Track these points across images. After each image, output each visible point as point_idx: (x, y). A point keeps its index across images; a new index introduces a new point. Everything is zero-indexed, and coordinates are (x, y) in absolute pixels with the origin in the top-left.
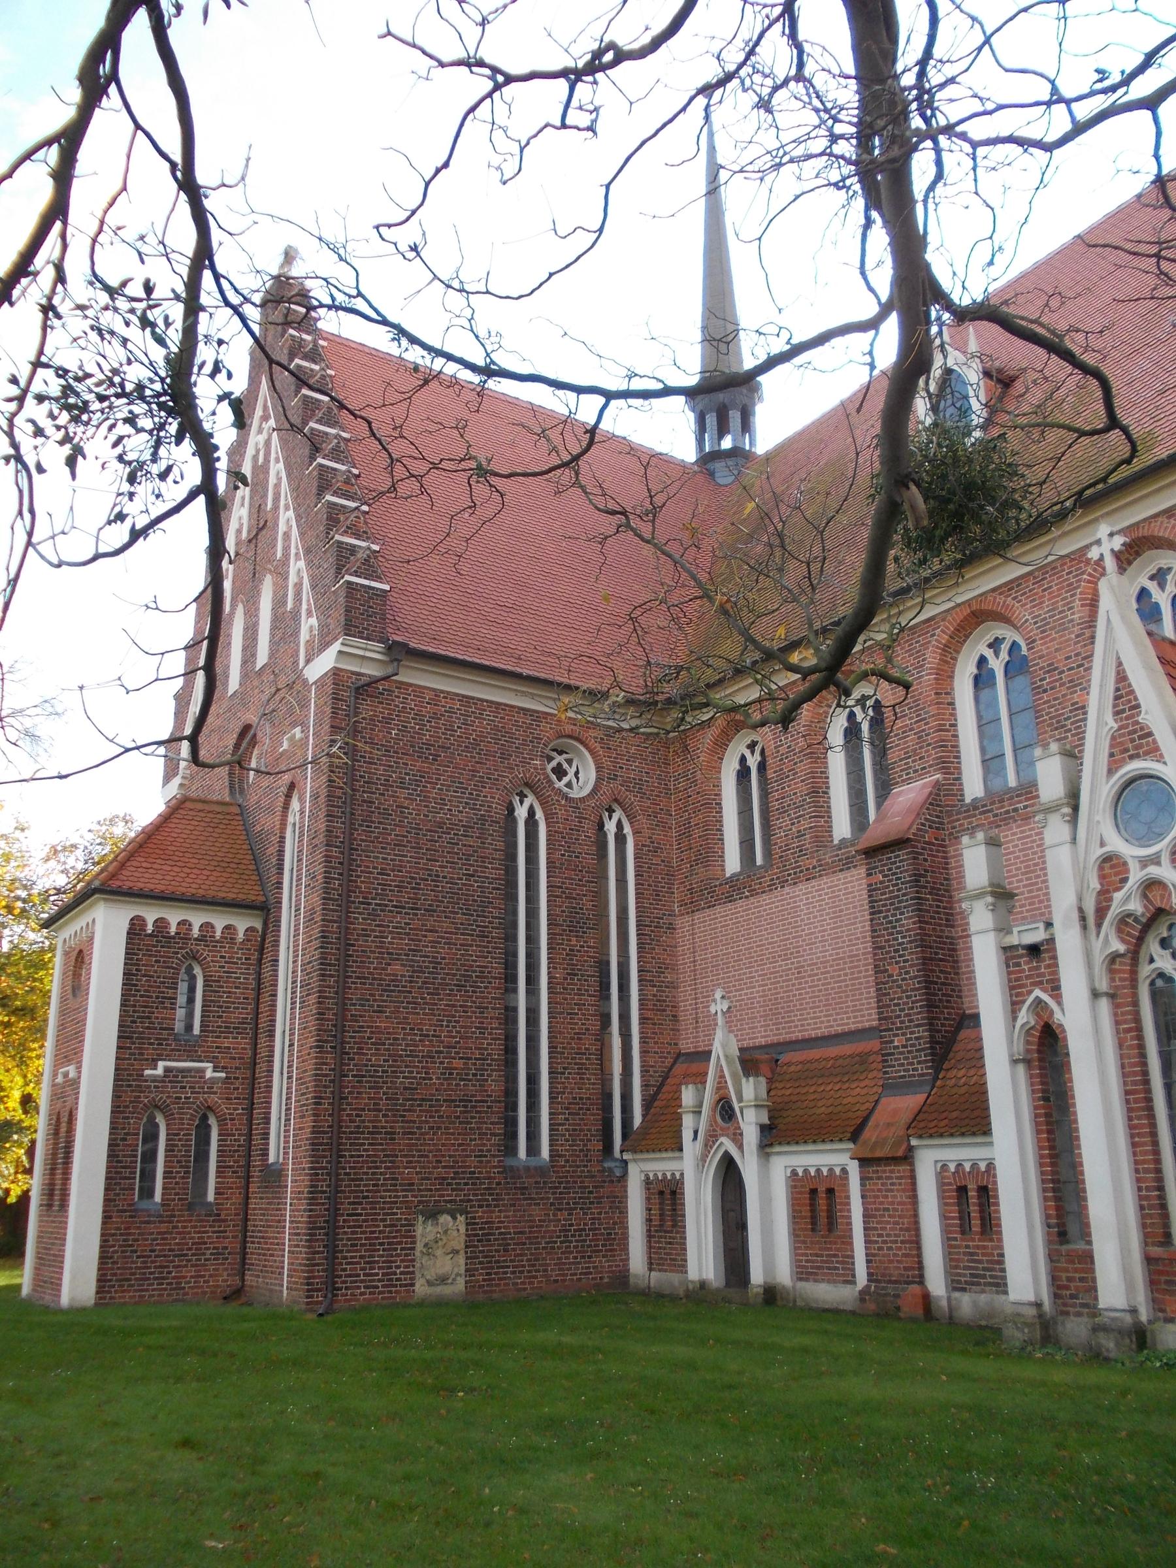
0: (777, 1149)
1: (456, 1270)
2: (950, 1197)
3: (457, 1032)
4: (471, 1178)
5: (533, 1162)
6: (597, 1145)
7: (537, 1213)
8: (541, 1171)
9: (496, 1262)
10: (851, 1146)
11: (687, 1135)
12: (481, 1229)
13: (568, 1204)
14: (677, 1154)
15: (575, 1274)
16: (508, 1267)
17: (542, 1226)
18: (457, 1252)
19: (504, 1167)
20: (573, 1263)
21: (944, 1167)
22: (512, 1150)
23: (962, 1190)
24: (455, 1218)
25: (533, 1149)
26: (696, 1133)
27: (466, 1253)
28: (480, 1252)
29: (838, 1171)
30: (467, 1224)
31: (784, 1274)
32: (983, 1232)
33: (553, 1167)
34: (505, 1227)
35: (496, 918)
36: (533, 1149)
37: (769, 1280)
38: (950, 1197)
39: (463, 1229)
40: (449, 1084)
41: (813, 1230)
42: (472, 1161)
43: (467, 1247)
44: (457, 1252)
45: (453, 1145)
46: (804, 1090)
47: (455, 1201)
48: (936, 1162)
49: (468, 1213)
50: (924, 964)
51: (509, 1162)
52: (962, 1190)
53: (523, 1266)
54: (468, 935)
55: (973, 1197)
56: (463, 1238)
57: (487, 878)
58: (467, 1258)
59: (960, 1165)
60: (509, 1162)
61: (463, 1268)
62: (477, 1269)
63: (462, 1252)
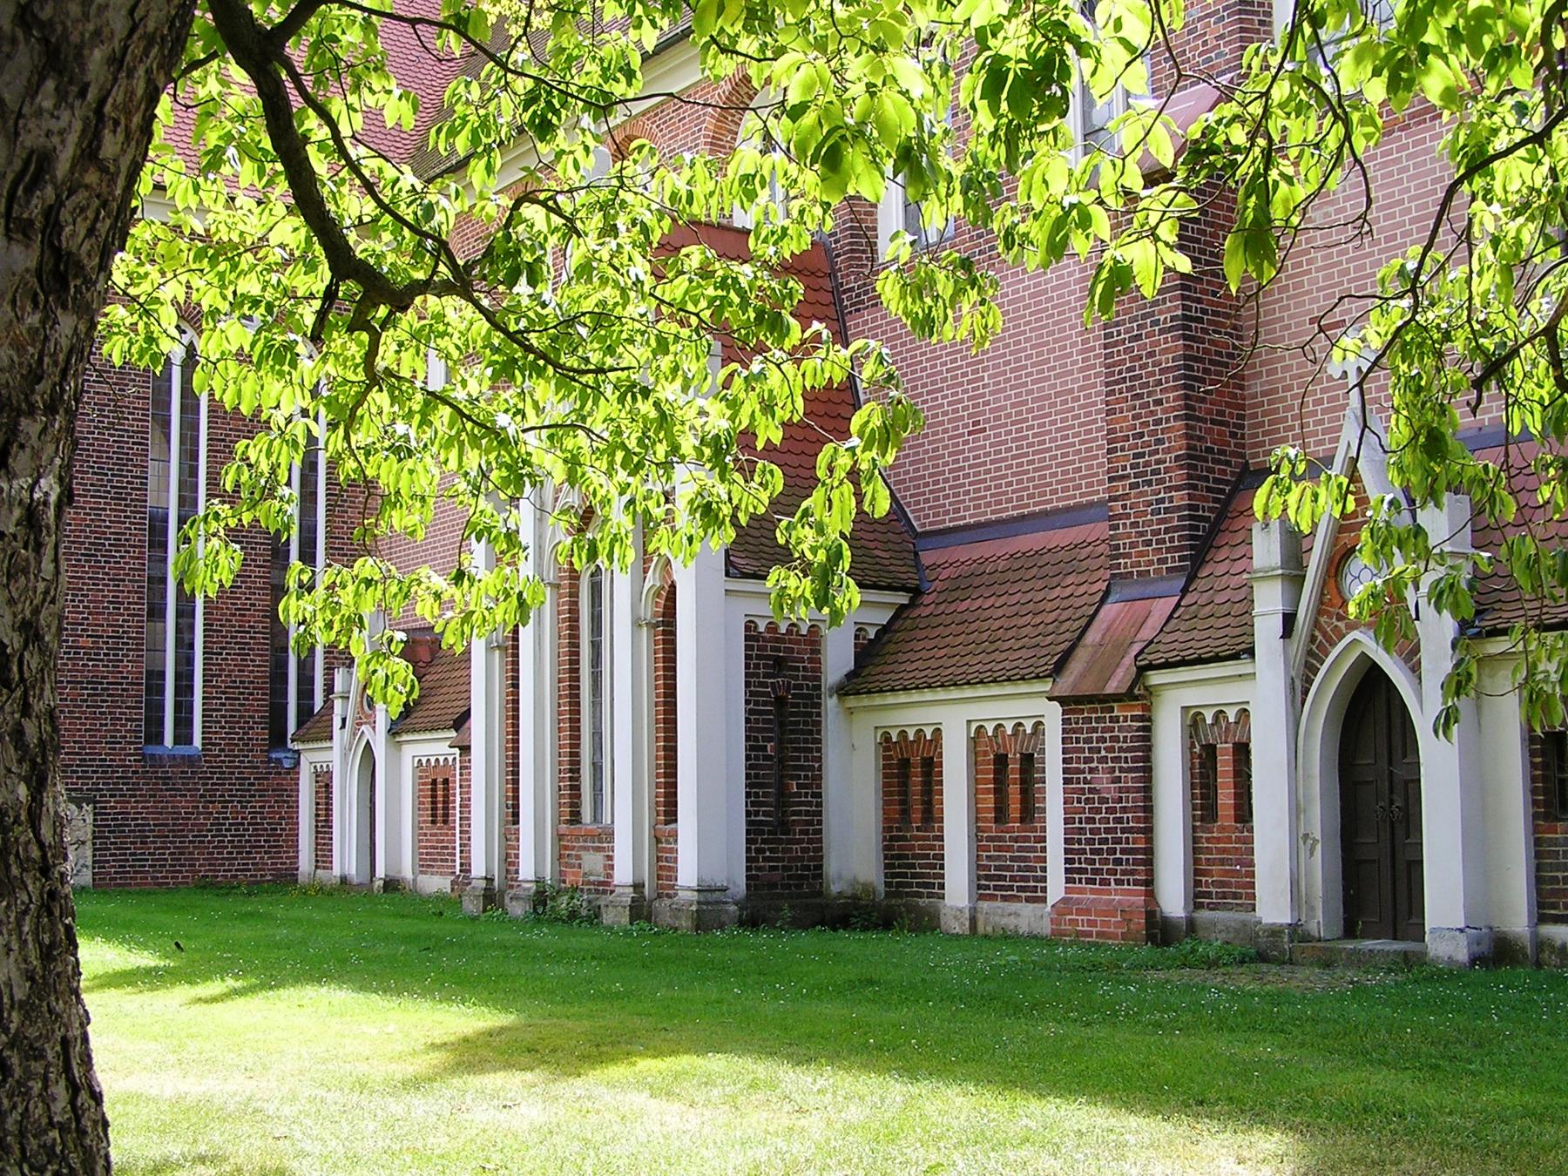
0: (405, 737)
1: (81, 862)
2: (424, 797)
3: (84, 607)
4: (101, 766)
5: (183, 750)
6: (261, 733)
7: (183, 805)
8: (190, 760)
9: (131, 854)
10: (453, 734)
11: (1267, 629)
12: (112, 820)
13: (223, 796)
14: (328, 744)
15: (231, 870)
16: (147, 860)
17: (189, 819)
18: (84, 843)
19: (143, 755)
20: (227, 859)
21: (887, 737)
22: (156, 737)
23: (1001, 761)
24: (80, 808)
25: (183, 736)
26: (344, 720)
27: (94, 844)
28: (112, 843)
29: (1231, 715)
30: (95, 814)
31: (407, 871)
32: (1022, 820)
33: (205, 756)
34: (142, 819)
35: (137, 477)
36: (183, 736)
37: (392, 874)
38: (424, 797)
39: (90, 819)
40: (74, 665)
41: (433, 822)
42: (103, 748)
43: (94, 838)
44: (84, 843)
45: (80, 730)
46: (1040, 596)
47: (81, 789)
48: (969, 722)
49: (96, 802)
50: (1187, 407)
51: (152, 749)
52: (1001, 761)
53: (166, 860)
54: (100, 497)
55: (1225, 763)
56: (90, 829)
57: (127, 431)
58: (95, 850)
59: (1020, 724)
60: (152, 749)
61: (89, 862)
62: (108, 861)
63: (89, 844)
